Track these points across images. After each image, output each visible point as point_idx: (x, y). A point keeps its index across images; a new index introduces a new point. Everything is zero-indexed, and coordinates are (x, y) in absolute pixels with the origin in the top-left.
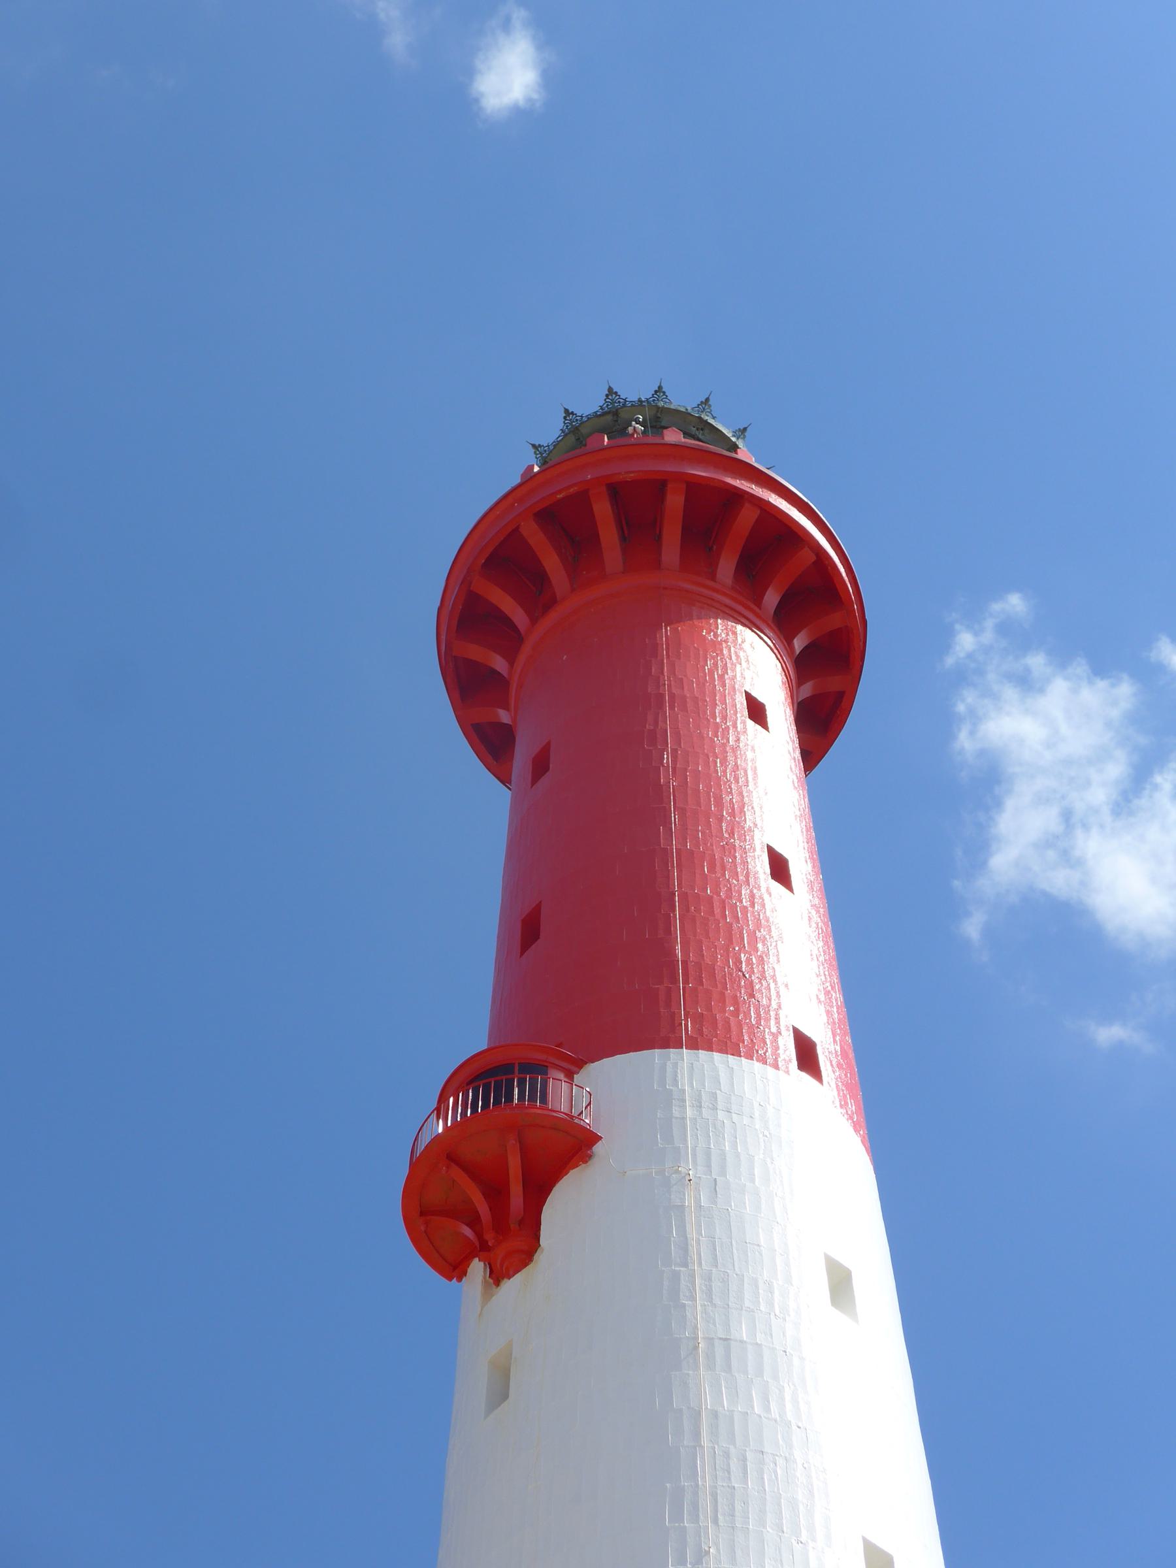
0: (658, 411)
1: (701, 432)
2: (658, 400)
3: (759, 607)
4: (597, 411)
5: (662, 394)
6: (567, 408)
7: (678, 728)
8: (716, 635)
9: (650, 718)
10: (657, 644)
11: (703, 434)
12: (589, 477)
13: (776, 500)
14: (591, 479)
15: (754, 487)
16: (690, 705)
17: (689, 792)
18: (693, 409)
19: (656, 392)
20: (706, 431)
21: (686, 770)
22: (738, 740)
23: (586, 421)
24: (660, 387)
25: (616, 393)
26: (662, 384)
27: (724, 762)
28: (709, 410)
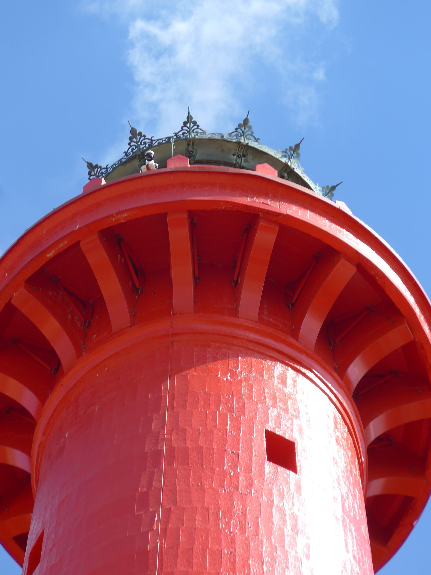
0: (189, 145)
1: (243, 159)
2: (188, 132)
3: (296, 338)
4: (122, 159)
5: (192, 125)
6: (89, 161)
7: (175, 485)
8: (234, 375)
9: (144, 481)
10: (161, 396)
11: (246, 161)
12: (78, 226)
13: (297, 212)
14: (79, 229)
15: (269, 202)
16: (192, 455)
17: (180, 553)
18: (230, 135)
19: (185, 123)
20: (250, 157)
21: (178, 529)
22: (250, 485)
23: (112, 171)
24: (189, 118)
25: (140, 134)
26: (191, 114)
27: (229, 512)
28: (250, 133)
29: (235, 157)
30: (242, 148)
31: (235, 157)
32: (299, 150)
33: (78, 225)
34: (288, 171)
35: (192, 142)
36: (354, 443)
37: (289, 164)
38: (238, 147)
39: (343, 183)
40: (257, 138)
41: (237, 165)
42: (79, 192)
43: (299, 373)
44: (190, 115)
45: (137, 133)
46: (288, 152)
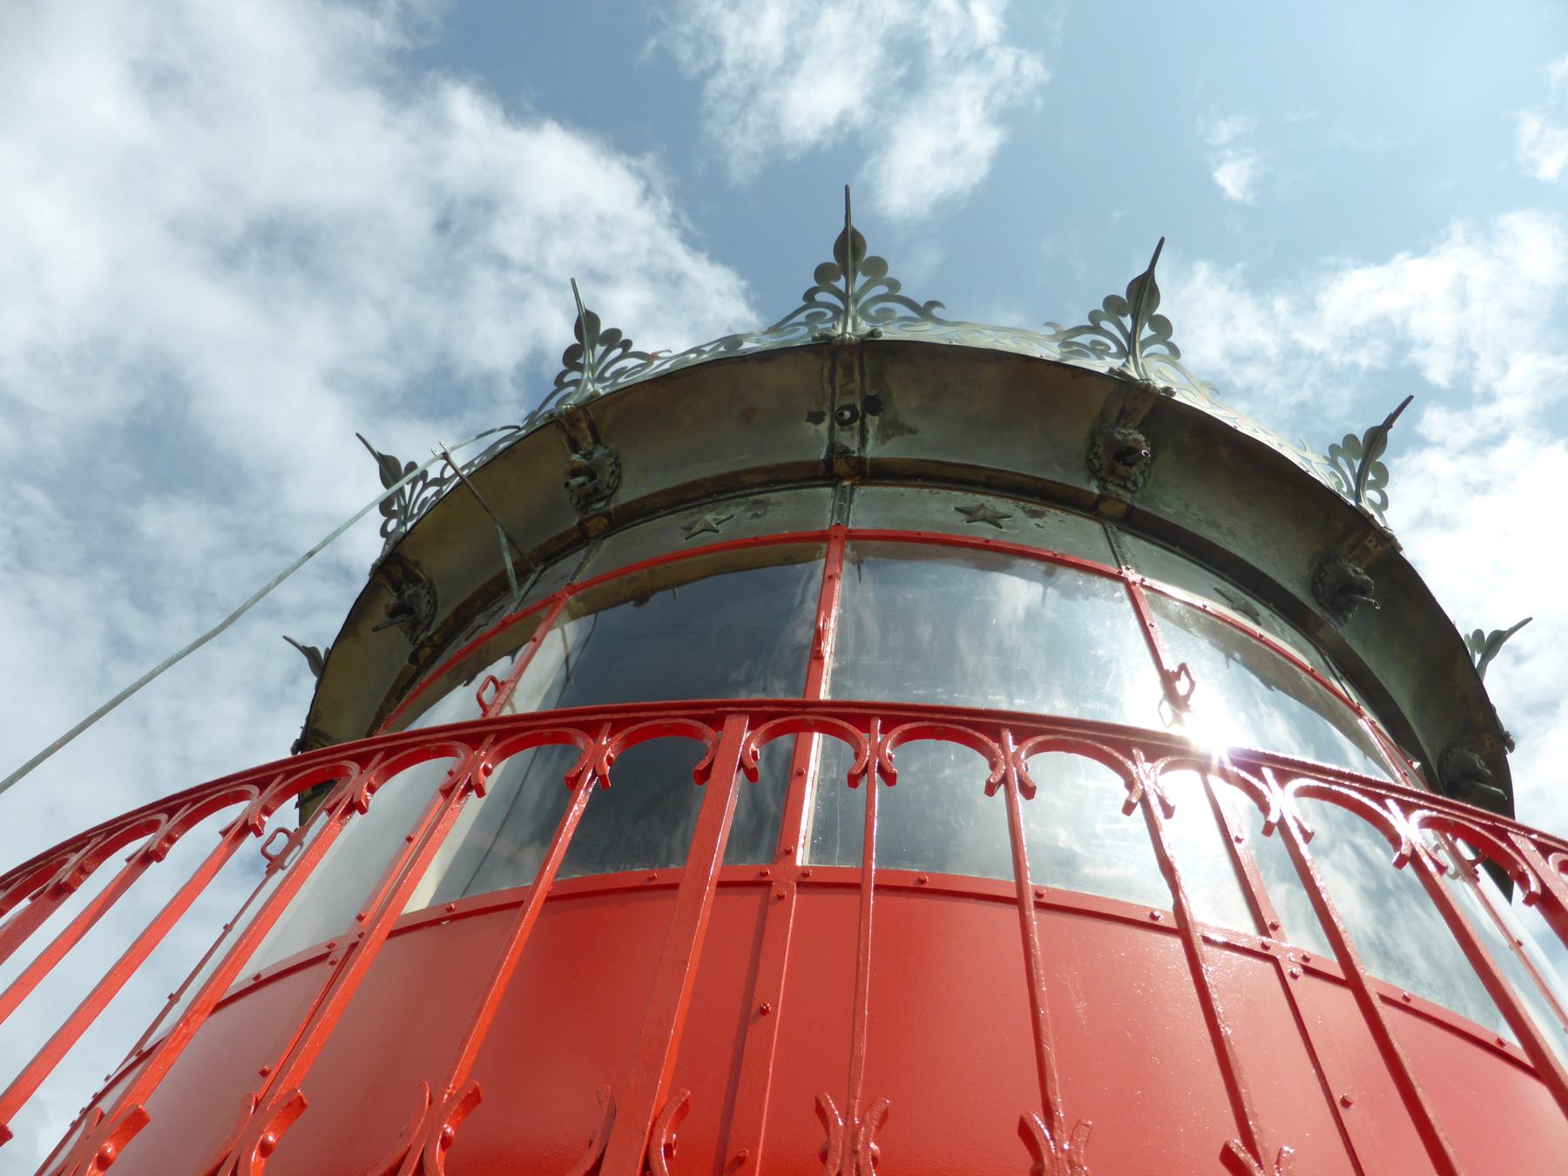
1: (873, 422)
26: (856, 223)
28: (882, 290)
29: (824, 427)
30: (848, 368)
31: (824, 427)
35: (584, 425)
37: (1133, 373)
38: (826, 372)
40: (922, 303)
41: (840, 467)
44: (855, 233)
45: (865, 258)
46: (1107, 325)
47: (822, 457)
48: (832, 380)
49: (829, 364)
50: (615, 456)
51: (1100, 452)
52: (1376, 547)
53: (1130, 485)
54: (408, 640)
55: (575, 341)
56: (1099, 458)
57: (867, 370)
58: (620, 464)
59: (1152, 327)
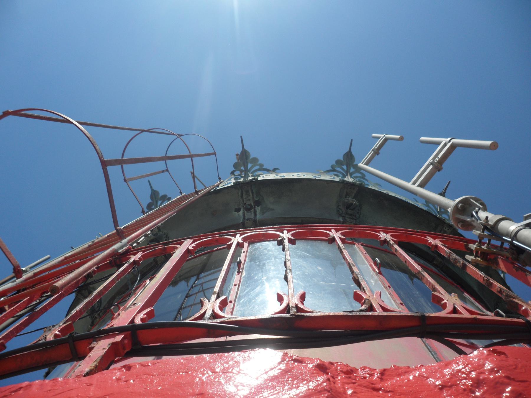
28: (258, 167)
29: (241, 213)
30: (247, 192)
32: (354, 161)
33: (104, 329)
34: (353, 195)
36: (137, 129)
39: (353, 140)
42: (75, 297)
43: (423, 338)
47: (241, 221)
48: (242, 197)
49: (240, 191)
50: (166, 234)
51: (341, 207)
52: (448, 230)
53: (354, 217)
54: (90, 318)
55: (151, 201)
56: (341, 210)
57: (254, 191)
58: (168, 237)
59: (354, 168)
